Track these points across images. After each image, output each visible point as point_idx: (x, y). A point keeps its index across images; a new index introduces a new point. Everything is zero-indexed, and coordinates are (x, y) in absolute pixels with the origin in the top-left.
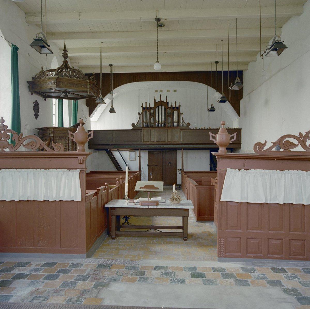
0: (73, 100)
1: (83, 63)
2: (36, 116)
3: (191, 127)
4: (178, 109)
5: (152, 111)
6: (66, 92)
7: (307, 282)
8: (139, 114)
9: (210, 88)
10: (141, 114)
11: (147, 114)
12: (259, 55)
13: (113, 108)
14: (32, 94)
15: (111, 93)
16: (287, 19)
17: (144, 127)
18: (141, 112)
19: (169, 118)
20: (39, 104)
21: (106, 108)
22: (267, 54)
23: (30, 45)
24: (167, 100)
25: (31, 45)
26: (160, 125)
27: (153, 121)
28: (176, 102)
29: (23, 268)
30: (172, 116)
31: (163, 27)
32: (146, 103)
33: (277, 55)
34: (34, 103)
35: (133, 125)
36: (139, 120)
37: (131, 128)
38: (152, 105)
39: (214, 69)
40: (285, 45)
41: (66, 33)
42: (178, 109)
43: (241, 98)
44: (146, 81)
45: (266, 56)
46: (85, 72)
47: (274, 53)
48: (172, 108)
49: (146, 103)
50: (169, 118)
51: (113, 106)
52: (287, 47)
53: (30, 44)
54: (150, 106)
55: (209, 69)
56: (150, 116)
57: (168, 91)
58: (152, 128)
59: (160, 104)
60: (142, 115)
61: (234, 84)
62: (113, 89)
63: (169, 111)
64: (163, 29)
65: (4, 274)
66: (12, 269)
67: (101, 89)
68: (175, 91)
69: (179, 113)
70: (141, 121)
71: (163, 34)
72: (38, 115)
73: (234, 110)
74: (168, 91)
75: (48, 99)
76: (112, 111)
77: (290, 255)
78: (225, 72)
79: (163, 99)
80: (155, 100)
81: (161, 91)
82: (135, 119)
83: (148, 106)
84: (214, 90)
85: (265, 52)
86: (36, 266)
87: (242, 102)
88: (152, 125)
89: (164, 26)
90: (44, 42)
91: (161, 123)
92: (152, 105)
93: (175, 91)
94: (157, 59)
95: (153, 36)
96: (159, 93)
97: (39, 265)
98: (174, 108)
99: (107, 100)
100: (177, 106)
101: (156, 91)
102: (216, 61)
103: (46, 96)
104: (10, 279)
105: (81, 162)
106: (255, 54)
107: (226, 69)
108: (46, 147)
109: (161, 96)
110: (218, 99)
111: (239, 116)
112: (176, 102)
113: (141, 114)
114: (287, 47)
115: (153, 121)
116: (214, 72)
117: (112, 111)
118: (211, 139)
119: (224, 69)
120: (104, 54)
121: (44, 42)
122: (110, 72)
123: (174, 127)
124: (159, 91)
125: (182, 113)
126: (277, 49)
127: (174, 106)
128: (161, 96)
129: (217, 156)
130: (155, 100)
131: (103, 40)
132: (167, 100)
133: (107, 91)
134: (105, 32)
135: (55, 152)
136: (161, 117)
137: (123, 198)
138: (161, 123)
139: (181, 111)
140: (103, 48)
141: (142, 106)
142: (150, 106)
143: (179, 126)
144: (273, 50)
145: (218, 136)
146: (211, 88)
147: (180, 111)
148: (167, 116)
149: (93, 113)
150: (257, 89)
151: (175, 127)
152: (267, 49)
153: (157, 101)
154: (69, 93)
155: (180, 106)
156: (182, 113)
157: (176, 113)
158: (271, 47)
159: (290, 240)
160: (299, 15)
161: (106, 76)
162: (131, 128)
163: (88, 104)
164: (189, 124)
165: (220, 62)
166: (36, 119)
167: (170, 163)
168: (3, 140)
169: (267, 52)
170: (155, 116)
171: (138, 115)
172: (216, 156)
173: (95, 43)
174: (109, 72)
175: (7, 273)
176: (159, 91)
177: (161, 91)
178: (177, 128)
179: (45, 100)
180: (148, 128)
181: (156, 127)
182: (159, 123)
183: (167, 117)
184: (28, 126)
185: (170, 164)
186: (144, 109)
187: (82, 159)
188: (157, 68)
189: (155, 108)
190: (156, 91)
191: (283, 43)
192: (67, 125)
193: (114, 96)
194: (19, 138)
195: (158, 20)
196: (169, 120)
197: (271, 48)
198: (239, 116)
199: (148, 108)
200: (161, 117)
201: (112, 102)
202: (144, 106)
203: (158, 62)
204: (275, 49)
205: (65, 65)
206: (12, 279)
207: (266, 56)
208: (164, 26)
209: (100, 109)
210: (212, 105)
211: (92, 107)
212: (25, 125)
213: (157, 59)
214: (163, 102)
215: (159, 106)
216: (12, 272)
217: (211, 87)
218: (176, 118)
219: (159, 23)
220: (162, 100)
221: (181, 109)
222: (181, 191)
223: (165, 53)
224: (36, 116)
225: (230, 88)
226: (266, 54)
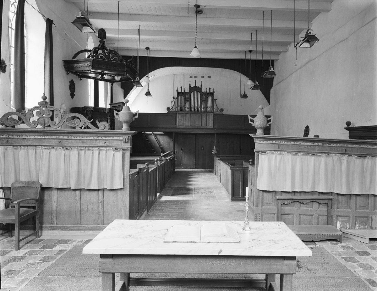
0: (109, 83)
1: (122, 45)
2: (72, 95)
3: (224, 113)
4: (212, 94)
5: (187, 96)
6: (102, 74)
7: (334, 252)
8: (174, 98)
9: (243, 76)
10: (176, 98)
11: (182, 98)
12: (292, 45)
13: (149, 91)
14: (68, 74)
15: (147, 77)
16: (318, 13)
17: (178, 111)
18: (176, 96)
19: (203, 104)
20: (75, 84)
21: (141, 91)
22: (301, 45)
23: (72, 23)
24: (201, 85)
25: (74, 23)
26: (193, 110)
27: (187, 106)
28: (210, 88)
29: (66, 245)
30: (206, 101)
31: (201, 13)
32: (181, 88)
33: (309, 46)
34: (70, 82)
35: (168, 109)
36: (174, 105)
37: (166, 112)
38: (187, 90)
39: (248, 57)
40: (317, 38)
41: (103, 13)
42: (212, 94)
43: (271, 86)
44: (182, 66)
45: (299, 47)
46: (122, 53)
47: (306, 45)
48: (206, 94)
49: (181, 88)
50: (203, 104)
51: (149, 89)
52: (319, 40)
53: (72, 22)
54: (185, 91)
55: (243, 57)
56: (185, 101)
57: (203, 77)
58: (187, 112)
59: (195, 89)
60: (177, 99)
61: (267, 73)
62: (150, 72)
63: (203, 97)
64: (201, 15)
65: (46, 250)
66: (54, 246)
67: (137, 72)
68: (209, 77)
69: (213, 99)
70: (176, 106)
71: (203, 21)
72: (74, 95)
73: (264, 98)
74: (203, 77)
75: (83, 79)
76: (148, 94)
77: (357, 209)
78: (259, 61)
79: (198, 85)
80: (190, 85)
81: (196, 77)
82: (170, 103)
83: (183, 91)
84: (247, 78)
85: (298, 43)
86: (78, 242)
87: (272, 90)
88: (187, 110)
89: (202, 12)
90: (86, 20)
91: (195, 108)
92: (187, 90)
93: (209, 77)
94: (196, 45)
95: (192, 22)
96: (194, 79)
97: (81, 242)
98: (208, 94)
99: (143, 81)
100: (211, 91)
101: (191, 77)
102: (250, 50)
103: (83, 75)
104: (54, 255)
105: (127, 141)
106: (287, 44)
107: (259, 57)
108: (90, 125)
109: (196, 81)
110: (251, 86)
111: (270, 104)
112: (210, 88)
113: (176, 98)
114: (319, 40)
115: (187, 106)
116: (248, 61)
117: (148, 94)
118: (250, 122)
119: (253, 58)
120: (141, 37)
121: (86, 20)
122: (146, 56)
123: (207, 112)
124: (193, 77)
125: (216, 99)
126: (310, 41)
127: (208, 92)
128: (196, 81)
129: (255, 137)
130: (190, 85)
131: (141, 23)
132: (201, 85)
133: (144, 73)
134: (144, 15)
135: (101, 130)
136: (195, 101)
137: (23, 226)
138: (195, 108)
139: (215, 97)
140: (140, 31)
141: (177, 91)
142: (185, 91)
143: (213, 112)
144: (306, 42)
145: (255, 119)
146: (244, 76)
147: (214, 97)
148: (201, 101)
149: (129, 94)
150: (287, 78)
151: (209, 112)
152: (300, 41)
153: (192, 86)
154: (105, 75)
155: (214, 92)
156: (216, 99)
157: (210, 99)
158: (304, 38)
159: (319, 215)
160: (328, 11)
161: (143, 59)
162: (166, 112)
163: (122, 87)
164: (222, 110)
165: (253, 51)
166: (72, 99)
167: (203, 147)
168: (44, 117)
169: (300, 43)
170: (190, 101)
171: (172, 99)
172: (253, 138)
173: (133, 25)
174: (145, 55)
175: (49, 250)
176: (193, 77)
177: (196, 77)
178: (211, 113)
179: (81, 79)
180: (183, 113)
181: (191, 111)
182: (194, 108)
183: (201, 102)
184: (64, 105)
185: (202, 148)
186: (179, 94)
187: (127, 138)
188: (195, 54)
189: (190, 93)
190: (191, 77)
191: (315, 36)
192: (102, 105)
193: (150, 79)
194: (62, 115)
195: (197, 6)
196: (203, 105)
197: (304, 40)
198: (270, 104)
199: (183, 93)
200: (195, 101)
201: (148, 85)
202: (180, 91)
203: (196, 47)
204: (307, 41)
205: (102, 46)
206: (55, 255)
207: (299, 47)
208: (202, 12)
209: (135, 92)
210: (245, 92)
211: (127, 91)
212: (61, 105)
213: (196, 45)
214: (198, 87)
215: (194, 92)
216: (54, 249)
217: (244, 75)
218: (210, 104)
219: (198, 10)
220: (197, 86)
221: (215, 94)
222: (214, 174)
223: (202, 39)
224: (72, 95)
225: (264, 76)
226: (299, 45)
